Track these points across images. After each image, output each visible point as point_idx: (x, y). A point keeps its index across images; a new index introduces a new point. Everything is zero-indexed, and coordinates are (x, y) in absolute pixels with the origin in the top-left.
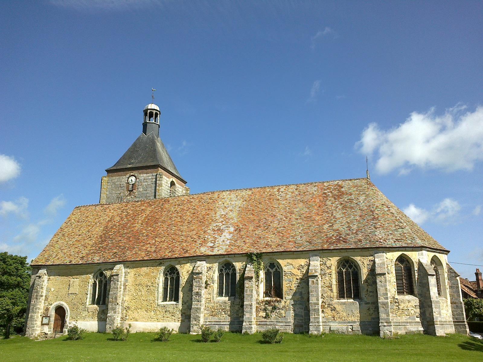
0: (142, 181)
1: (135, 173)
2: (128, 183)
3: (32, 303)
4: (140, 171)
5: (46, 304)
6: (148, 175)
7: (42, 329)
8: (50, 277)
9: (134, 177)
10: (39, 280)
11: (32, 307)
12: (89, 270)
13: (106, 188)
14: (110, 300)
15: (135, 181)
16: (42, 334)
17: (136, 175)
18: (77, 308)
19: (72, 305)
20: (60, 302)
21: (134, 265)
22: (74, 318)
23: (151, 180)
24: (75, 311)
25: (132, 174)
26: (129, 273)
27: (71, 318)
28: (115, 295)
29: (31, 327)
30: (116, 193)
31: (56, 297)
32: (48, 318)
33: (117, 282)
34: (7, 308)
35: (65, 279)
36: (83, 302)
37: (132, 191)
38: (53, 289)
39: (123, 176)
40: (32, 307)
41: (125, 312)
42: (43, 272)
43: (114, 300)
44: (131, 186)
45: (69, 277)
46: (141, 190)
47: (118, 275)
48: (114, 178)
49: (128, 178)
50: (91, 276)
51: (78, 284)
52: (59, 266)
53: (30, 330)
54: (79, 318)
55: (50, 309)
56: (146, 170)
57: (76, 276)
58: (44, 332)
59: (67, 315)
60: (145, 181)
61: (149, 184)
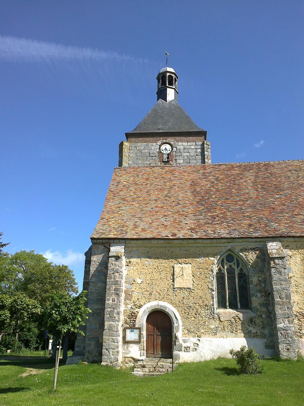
0: (182, 151)
1: (171, 140)
2: (160, 152)
3: (109, 302)
4: (177, 138)
5: (129, 306)
6: (189, 144)
7: (127, 352)
8: (130, 260)
9: (169, 146)
10: (117, 263)
11: (109, 310)
12: (209, 250)
13: (128, 156)
14: (277, 299)
15: (171, 150)
16: (127, 359)
17: (172, 143)
18: (196, 314)
19: (186, 308)
20: (158, 303)
21: (299, 244)
22: (193, 332)
23: (195, 150)
24: (193, 319)
25: (165, 141)
26: (290, 256)
27: (187, 332)
28: (286, 291)
29: (113, 347)
30: (144, 163)
31: (149, 293)
32: (137, 331)
33: (283, 270)
34: (34, 311)
35: (165, 263)
36: (207, 303)
37: (168, 162)
38: (139, 281)
39: (152, 142)
40: (109, 310)
41: (297, 322)
42: (115, 249)
43: (284, 300)
44: (165, 157)
45: (170, 260)
46: (181, 161)
47: (285, 257)
48: (139, 144)
49: (160, 146)
50: (215, 260)
51: (191, 272)
52: (153, 241)
53: (111, 353)
54: (202, 331)
55: (140, 315)
56: (185, 137)
57: (185, 259)
58: (132, 358)
59: (178, 327)
60: (185, 150)
61: (192, 155)
